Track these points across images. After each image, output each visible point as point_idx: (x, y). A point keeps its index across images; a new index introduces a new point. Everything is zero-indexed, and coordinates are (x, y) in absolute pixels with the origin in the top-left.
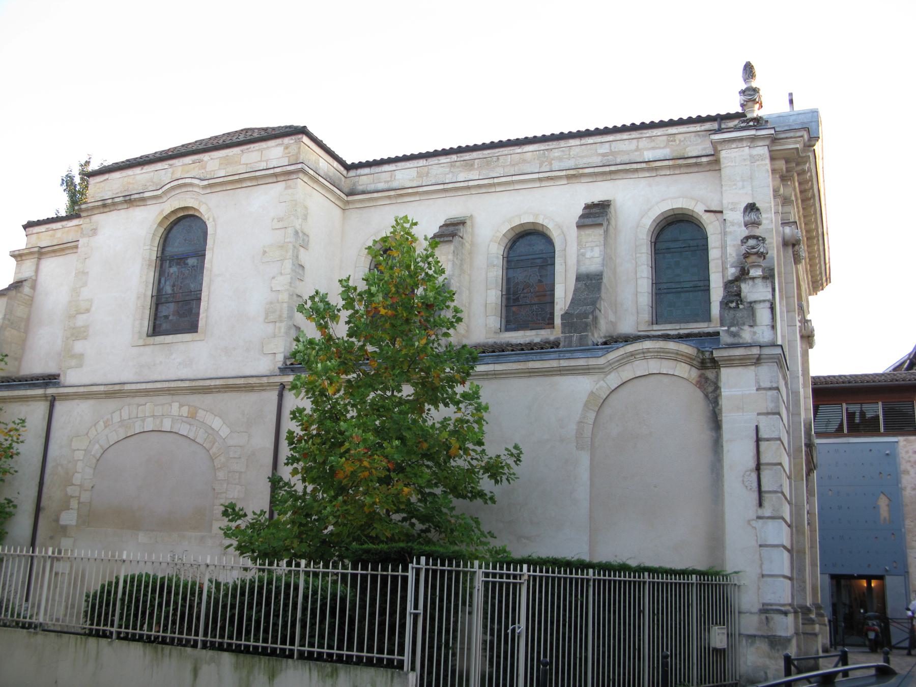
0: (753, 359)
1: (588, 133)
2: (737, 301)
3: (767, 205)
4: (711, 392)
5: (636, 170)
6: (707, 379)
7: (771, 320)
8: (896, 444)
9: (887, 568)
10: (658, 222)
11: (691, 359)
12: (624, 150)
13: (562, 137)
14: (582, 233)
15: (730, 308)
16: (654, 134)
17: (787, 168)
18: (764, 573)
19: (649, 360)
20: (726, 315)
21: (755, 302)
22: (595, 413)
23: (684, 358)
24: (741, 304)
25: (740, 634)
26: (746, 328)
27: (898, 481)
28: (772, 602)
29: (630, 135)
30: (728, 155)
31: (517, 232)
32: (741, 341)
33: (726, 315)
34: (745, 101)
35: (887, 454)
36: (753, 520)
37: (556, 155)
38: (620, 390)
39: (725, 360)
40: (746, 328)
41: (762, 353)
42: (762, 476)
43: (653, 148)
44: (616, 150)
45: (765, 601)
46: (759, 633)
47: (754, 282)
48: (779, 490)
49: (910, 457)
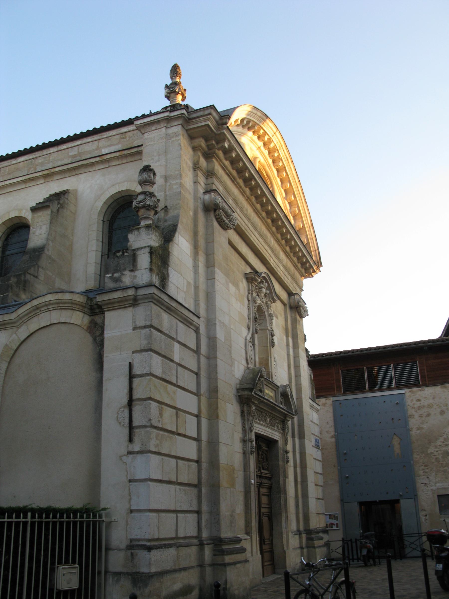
0: (130, 300)
1: (63, 141)
2: (123, 250)
3: (177, 172)
4: (99, 336)
5: (93, 164)
6: (96, 324)
7: (149, 264)
8: (403, 395)
9: (401, 494)
10: (109, 204)
11: (82, 306)
12: (88, 150)
13: (45, 146)
14: (35, 215)
15: (117, 256)
16: (111, 135)
17: (208, 146)
18: (133, 508)
19: (52, 312)
20: (111, 263)
21: (138, 249)
22: (7, 364)
23: (78, 307)
24: (126, 252)
25: (106, 572)
26: (127, 273)
27: (406, 424)
28: (139, 537)
29: (93, 138)
30: (149, 137)
31: (9, 226)
32: (122, 285)
33: (111, 263)
34: (168, 93)
35: (397, 404)
36: (125, 455)
37: (40, 161)
38: (28, 341)
39: (107, 304)
40: (127, 273)
41: (138, 294)
42: (133, 412)
43: (110, 146)
44: (82, 151)
45: (132, 537)
46: (125, 570)
47: (138, 231)
48: (148, 424)
49: (414, 404)
